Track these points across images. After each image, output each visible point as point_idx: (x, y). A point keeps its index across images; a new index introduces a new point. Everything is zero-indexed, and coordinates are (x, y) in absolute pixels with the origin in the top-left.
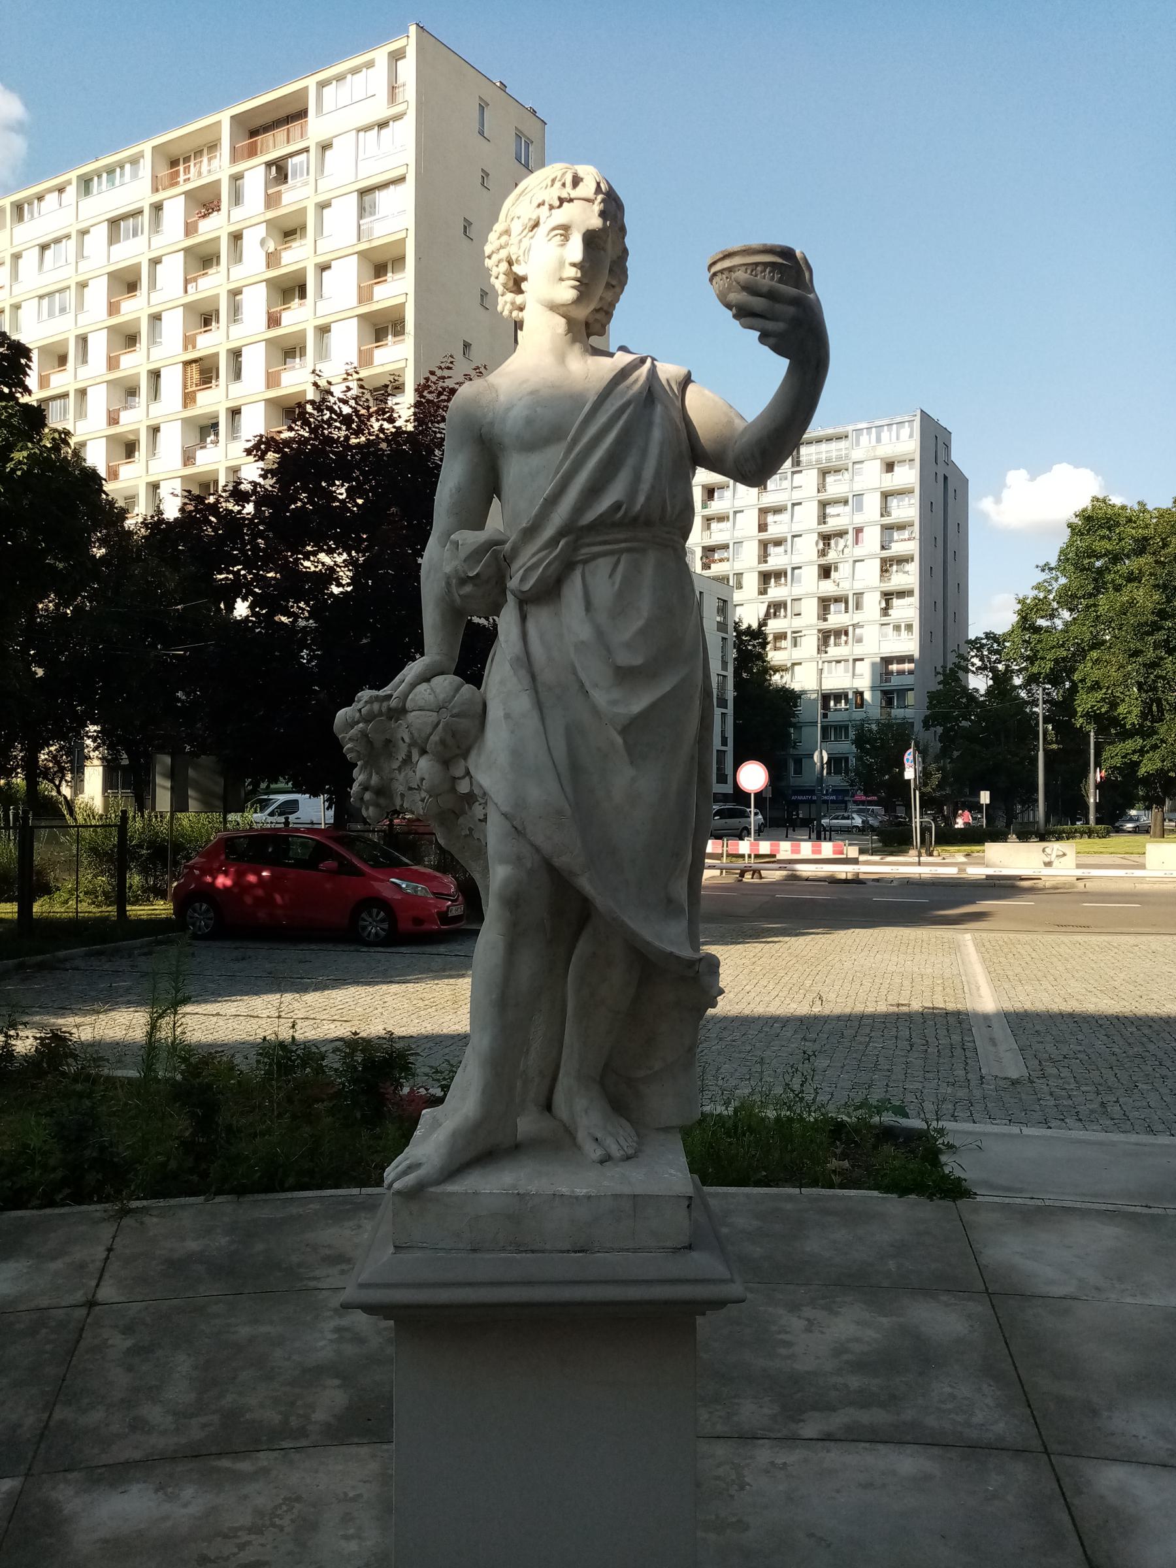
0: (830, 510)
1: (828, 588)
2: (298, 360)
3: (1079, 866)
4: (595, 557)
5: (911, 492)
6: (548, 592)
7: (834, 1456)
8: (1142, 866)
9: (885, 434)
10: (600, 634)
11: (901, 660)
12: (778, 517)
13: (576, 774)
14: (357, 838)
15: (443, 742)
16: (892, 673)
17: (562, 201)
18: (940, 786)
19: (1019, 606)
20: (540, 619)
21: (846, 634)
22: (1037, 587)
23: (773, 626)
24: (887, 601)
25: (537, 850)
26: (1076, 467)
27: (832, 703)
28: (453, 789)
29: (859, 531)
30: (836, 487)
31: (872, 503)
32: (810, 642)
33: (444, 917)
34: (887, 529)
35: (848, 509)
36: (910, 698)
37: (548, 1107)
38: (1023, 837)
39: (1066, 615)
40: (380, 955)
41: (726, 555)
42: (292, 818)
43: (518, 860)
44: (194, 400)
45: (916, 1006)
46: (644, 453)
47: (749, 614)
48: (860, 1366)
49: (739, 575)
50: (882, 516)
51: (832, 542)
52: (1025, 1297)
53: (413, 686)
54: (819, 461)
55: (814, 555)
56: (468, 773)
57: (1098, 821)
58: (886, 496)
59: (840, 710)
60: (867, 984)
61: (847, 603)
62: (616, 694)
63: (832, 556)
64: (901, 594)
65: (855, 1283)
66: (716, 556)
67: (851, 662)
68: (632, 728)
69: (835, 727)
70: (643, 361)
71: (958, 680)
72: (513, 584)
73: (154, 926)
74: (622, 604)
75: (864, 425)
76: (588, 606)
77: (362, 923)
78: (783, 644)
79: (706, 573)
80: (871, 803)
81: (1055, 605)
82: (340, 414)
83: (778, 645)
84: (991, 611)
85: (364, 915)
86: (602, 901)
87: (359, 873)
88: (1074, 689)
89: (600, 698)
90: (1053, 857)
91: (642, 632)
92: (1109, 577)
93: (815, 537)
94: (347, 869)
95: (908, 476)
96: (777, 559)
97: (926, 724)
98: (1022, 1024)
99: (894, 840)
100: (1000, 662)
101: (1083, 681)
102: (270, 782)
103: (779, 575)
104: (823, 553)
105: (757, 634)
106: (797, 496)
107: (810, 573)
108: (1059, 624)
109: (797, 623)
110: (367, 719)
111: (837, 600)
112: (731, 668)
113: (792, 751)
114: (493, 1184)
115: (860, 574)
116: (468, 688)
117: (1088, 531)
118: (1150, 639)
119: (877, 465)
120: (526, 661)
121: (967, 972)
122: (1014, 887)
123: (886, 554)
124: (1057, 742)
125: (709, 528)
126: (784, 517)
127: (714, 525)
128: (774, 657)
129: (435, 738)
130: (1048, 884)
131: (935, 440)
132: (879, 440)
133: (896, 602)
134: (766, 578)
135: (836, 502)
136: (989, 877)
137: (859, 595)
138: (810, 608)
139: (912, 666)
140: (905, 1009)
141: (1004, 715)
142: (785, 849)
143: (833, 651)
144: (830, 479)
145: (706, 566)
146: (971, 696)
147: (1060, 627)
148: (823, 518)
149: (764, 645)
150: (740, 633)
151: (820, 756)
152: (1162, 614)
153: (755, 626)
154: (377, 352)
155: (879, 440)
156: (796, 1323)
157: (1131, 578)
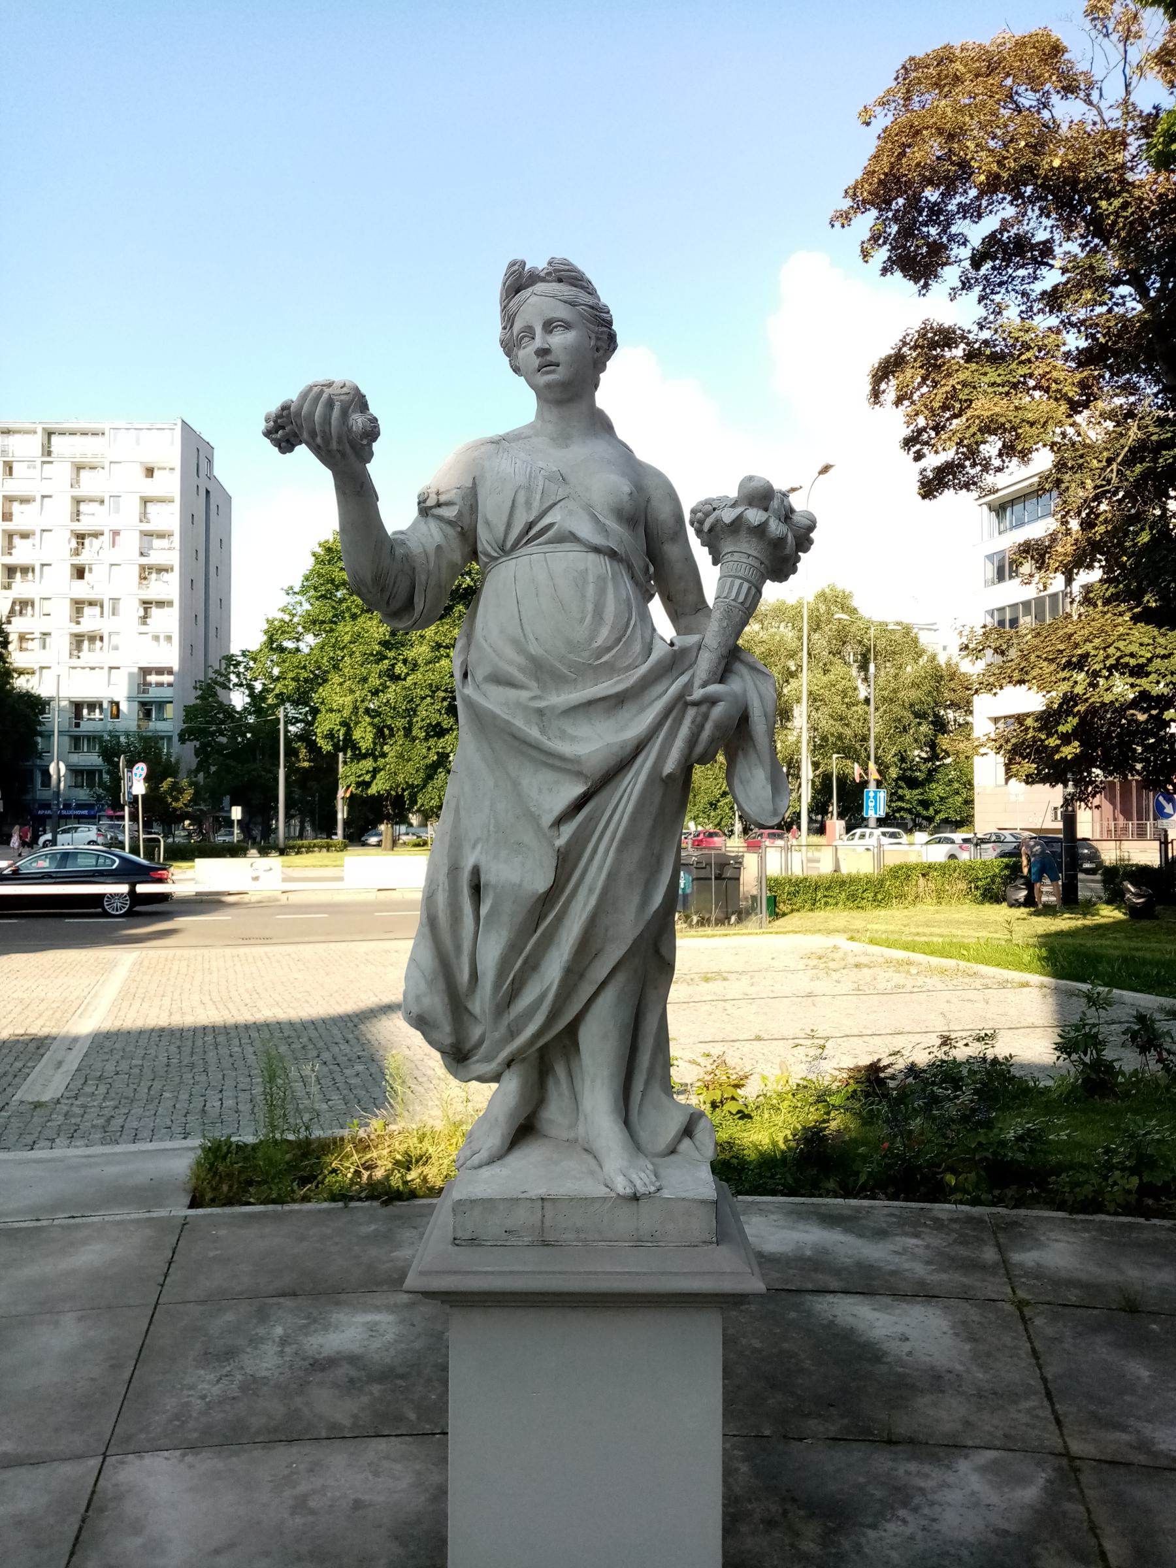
0: (83, 507)
1: (81, 589)
3: (284, 880)
8: (341, 879)
11: (160, 671)
12: (24, 507)
16: (150, 684)
19: (266, 626)
21: (101, 639)
24: (146, 609)
26: (794, 571)
27: (85, 711)
29: (116, 533)
30: (90, 484)
31: (133, 507)
32: (61, 643)
36: (169, 711)
50: (141, 521)
51: (87, 541)
59: (94, 720)
61: (102, 607)
64: (160, 604)
67: (106, 669)
69: (89, 738)
71: (215, 695)
78: (30, 645)
81: (300, 629)
83: (24, 645)
84: (245, 634)
95: (169, 483)
100: (256, 679)
103: (25, 570)
113: (38, 762)
115: (115, 575)
117: (329, 561)
123: (144, 561)
124: (309, 761)
128: (17, 658)
130: (254, 899)
136: (198, 894)
137: (115, 600)
139: (170, 679)
143: (88, 655)
144: (83, 473)
146: (229, 711)
151: (58, 769)
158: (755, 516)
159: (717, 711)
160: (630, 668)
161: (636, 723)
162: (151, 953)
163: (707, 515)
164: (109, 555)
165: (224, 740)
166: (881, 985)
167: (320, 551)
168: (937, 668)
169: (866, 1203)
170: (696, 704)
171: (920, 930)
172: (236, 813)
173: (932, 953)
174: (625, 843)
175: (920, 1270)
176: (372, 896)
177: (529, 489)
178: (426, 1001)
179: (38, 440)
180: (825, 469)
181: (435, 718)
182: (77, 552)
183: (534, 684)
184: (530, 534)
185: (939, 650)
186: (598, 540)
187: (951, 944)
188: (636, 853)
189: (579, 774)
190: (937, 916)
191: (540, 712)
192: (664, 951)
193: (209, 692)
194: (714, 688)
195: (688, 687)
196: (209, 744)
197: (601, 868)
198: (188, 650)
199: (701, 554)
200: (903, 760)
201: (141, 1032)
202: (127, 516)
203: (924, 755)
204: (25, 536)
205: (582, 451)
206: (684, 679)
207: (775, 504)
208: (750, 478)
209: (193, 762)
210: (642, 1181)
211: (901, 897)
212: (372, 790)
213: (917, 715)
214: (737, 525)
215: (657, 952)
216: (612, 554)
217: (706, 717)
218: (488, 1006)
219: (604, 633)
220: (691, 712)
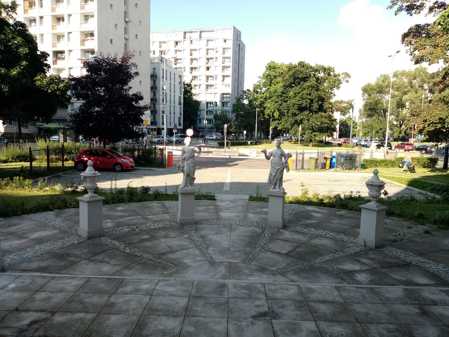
1: (208, 73)
11: (227, 94)
13: (189, 169)
18: (235, 129)
29: (217, 58)
31: (220, 51)
32: (203, 87)
33: (132, 167)
40: (120, 174)
44: (27, 12)
45: (217, 182)
47: (187, 79)
49: (185, 68)
51: (210, 60)
64: (227, 76)
71: (240, 101)
73: (70, 168)
78: (196, 87)
81: (262, 86)
87: (115, 158)
94: (112, 157)
95: (230, 44)
96: (195, 64)
98: (232, 184)
105: (189, 85)
112: (182, 94)
114: (185, 188)
115: (216, 70)
123: (223, 65)
125: (176, 53)
127: (178, 52)
128: (193, 91)
131: (237, 35)
134: (192, 69)
137: (216, 76)
138: (204, 78)
143: (210, 90)
144: (209, 42)
145: (176, 64)
148: (207, 53)
149: (191, 89)
150: (184, 84)
152: (283, 93)
154: (86, 6)
161: (280, 167)
162: (233, 169)
164: (215, 64)
172: (245, 132)
179: (198, 34)
180: (398, 52)
193: (239, 100)
196: (238, 114)
198: (233, 88)
201: (237, 183)
202: (220, 55)
204: (195, 59)
205: (279, 150)
209: (235, 118)
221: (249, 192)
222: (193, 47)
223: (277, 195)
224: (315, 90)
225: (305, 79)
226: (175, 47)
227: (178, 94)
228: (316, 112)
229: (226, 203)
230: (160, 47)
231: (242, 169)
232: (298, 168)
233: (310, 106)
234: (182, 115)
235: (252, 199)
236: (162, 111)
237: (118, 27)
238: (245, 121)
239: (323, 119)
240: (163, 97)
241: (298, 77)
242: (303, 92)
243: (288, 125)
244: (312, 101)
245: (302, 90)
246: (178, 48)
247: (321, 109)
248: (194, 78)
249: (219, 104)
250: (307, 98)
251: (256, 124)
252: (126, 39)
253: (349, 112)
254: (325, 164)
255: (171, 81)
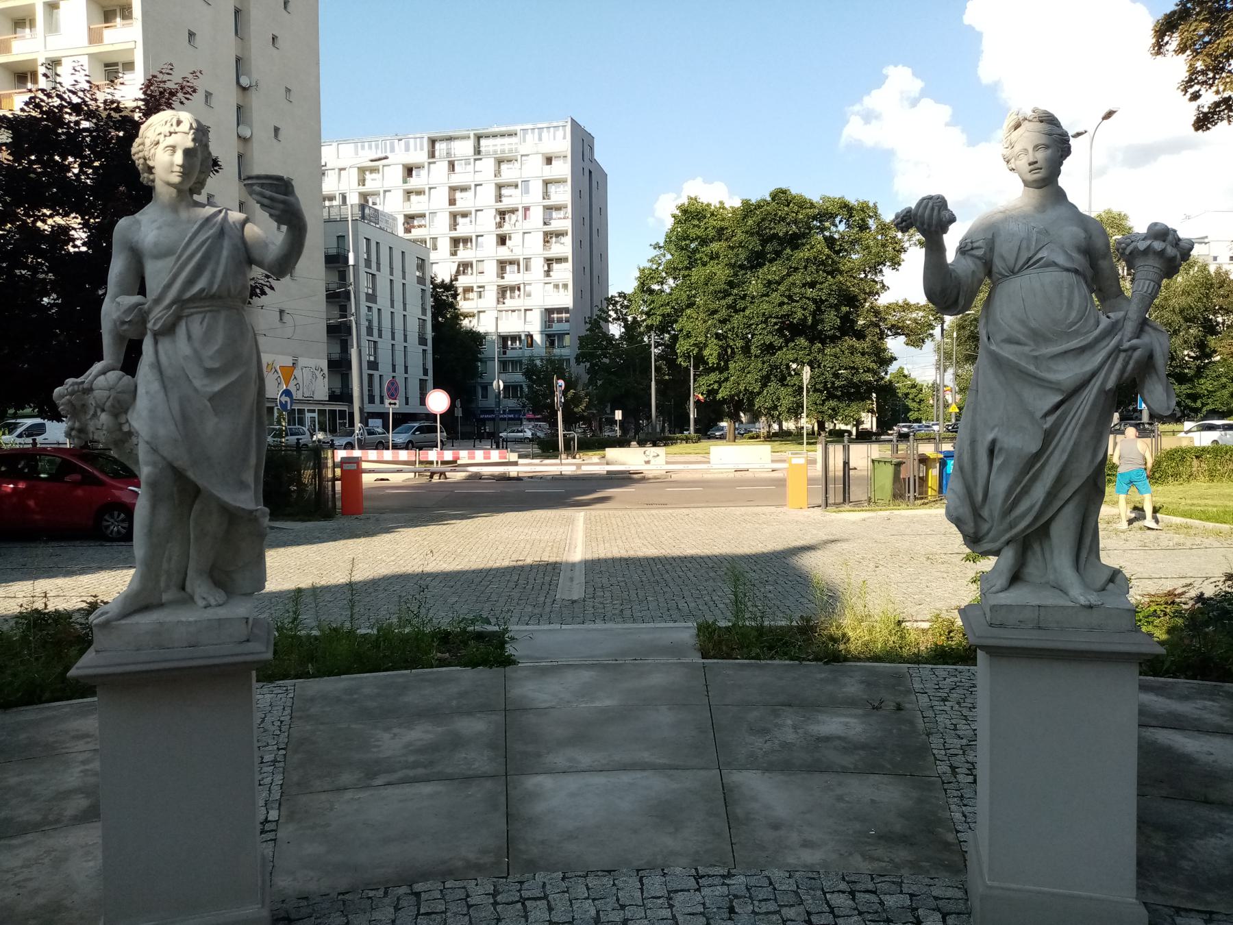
0: (504, 191)
1: (504, 253)
2: (28, 30)
4: (192, 314)
5: (565, 181)
6: (169, 330)
7: (390, 791)
9: (545, 134)
10: (195, 351)
11: (560, 311)
12: (464, 194)
13: (185, 420)
14: (99, 455)
15: (113, 406)
17: (171, 133)
20: (165, 345)
21: (519, 289)
22: (651, 261)
23: (462, 282)
24: (549, 265)
25: (164, 458)
28: (120, 429)
29: (527, 209)
30: (508, 173)
31: (536, 188)
32: (491, 295)
34: (548, 209)
35: (519, 191)
36: (567, 340)
37: (183, 588)
38: (642, 443)
39: (671, 281)
41: (423, 222)
42: (39, 439)
43: (154, 464)
45: (529, 561)
46: (218, 263)
47: (443, 271)
48: (420, 751)
49: (434, 239)
52: (525, 710)
53: (96, 377)
54: (495, 152)
55: (492, 226)
56: (127, 421)
57: (696, 431)
58: (546, 183)
60: (501, 548)
62: (206, 381)
63: (507, 228)
64: (559, 260)
65: (431, 714)
66: (416, 223)
68: (213, 398)
70: (220, 211)
71: (600, 327)
72: (149, 325)
74: (207, 338)
75: (530, 126)
76: (189, 337)
77: (106, 524)
78: (471, 295)
79: (408, 236)
80: (538, 420)
82: (70, 103)
84: (622, 279)
85: (106, 517)
86: (201, 483)
87: (102, 483)
88: (675, 339)
89: (197, 383)
90: (650, 458)
91: (218, 351)
92: (698, 256)
93: (493, 212)
94: (89, 480)
95: (563, 169)
96: (464, 228)
97: (578, 359)
98: (593, 567)
99: (548, 448)
101: (681, 330)
102: (17, 409)
103: (466, 240)
104: (500, 225)
105: (449, 287)
106: (479, 178)
107: (490, 241)
108: (667, 288)
109: (481, 280)
110: (72, 394)
111: (511, 263)
114: (146, 620)
115: (527, 242)
116: (127, 378)
118: (723, 302)
119: (540, 160)
120: (157, 366)
121: (570, 538)
122: (631, 479)
123: (547, 228)
125: (409, 200)
126: (470, 194)
127: (413, 197)
128: (464, 305)
129: (108, 404)
131: (583, 144)
132: (540, 139)
133: (555, 266)
134: (456, 242)
135: (509, 185)
136: (609, 472)
137: (527, 260)
138: (491, 268)
140: (520, 563)
141: (632, 355)
142: (464, 456)
143: (510, 303)
144: (504, 167)
145: (408, 231)
147: (668, 291)
148: (499, 198)
149: (455, 296)
150: (435, 286)
151: (498, 384)
152: (731, 284)
153: (447, 280)
155: (540, 139)
156: (387, 736)
157: (714, 257)
158: (1158, 245)
159: (1137, 354)
160: (1090, 332)
162: (593, 512)
163: (1128, 245)
165: (606, 361)
166: (1164, 543)
167: (678, 212)
168: (1207, 277)
169: (1171, 680)
170: (1125, 351)
171: (1195, 502)
172: (618, 415)
173: (1208, 519)
174: (1084, 426)
175: (1218, 719)
176: (732, 475)
177: (1029, 239)
178: (961, 510)
180: (1109, 114)
181: (769, 339)
182: (500, 225)
183: (1032, 343)
184: (1029, 264)
185: (1210, 260)
186: (1068, 265)
187: (1225, 512)
188: (1091, 430)
189: (1059, 390)
190: (1210, 491)
191: (1036, 358)
192: (1100, 485)
194: (1134, 341)
195: (1121, 342)
196: (596, 364)
197: (1069, 439)
198: (578, 294)
199: (1122, 270)
200: (1172, 358)
201: (614, 560)
202: (535, 194)
203: (1192, 354)
206: (1117, 338)
207: (1170, 237)
208: (1155, 224)
209: (585, 378)
210: (1093, 599)
211: (1176, 476)
212: (719, 396)
213: (1186, 320)
214: (1147, 251)
215: (1096, 484)
216: (1076, 272)
217: (1130, 357)
218: (996, 514)
219: (1074, 315)
220: (1122, 355)
221: (682, 604)
222: (457, 179)
223: (1079, 641)
224: (828, 273)
225: (794, 241)
226: (405, 182)
227: (414, 312)
228: (834, 339)
229: (574, 680)
230: (362, 182)
231: (624, 512)
232: (831, 501)
233: (816, 322)
234: (430, 372)
235: (717, 643)
236: (369, 362)
237: (214, 101)
238: (617, 383)
239: (858, 359)
240: (370, 321)
241: (775, 236)
242: (791, 279)
243: (751, 380)
244: (818, 303)
245: (788, 275)
246: (415, 182)
247: (847, 327)
248: (464, 267)
249: (538, 338)
250: (803, 296)
251: (653, 383)
252: (244, 140)
253: (932, 335)
254: (923, 480)
255: (392, 274)
